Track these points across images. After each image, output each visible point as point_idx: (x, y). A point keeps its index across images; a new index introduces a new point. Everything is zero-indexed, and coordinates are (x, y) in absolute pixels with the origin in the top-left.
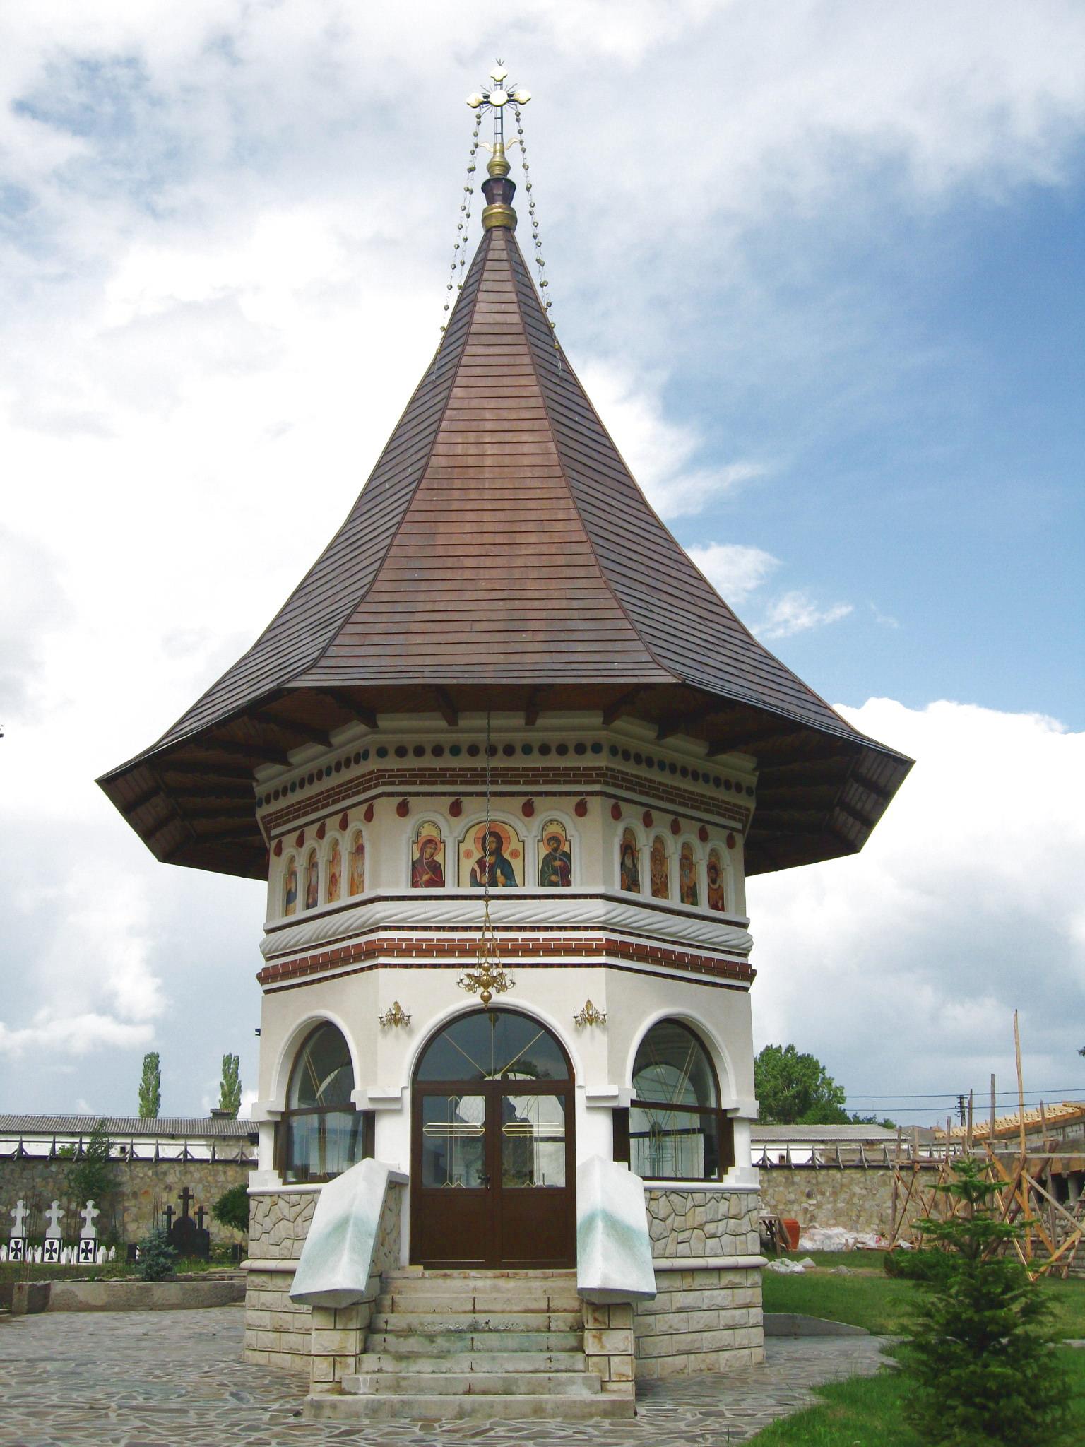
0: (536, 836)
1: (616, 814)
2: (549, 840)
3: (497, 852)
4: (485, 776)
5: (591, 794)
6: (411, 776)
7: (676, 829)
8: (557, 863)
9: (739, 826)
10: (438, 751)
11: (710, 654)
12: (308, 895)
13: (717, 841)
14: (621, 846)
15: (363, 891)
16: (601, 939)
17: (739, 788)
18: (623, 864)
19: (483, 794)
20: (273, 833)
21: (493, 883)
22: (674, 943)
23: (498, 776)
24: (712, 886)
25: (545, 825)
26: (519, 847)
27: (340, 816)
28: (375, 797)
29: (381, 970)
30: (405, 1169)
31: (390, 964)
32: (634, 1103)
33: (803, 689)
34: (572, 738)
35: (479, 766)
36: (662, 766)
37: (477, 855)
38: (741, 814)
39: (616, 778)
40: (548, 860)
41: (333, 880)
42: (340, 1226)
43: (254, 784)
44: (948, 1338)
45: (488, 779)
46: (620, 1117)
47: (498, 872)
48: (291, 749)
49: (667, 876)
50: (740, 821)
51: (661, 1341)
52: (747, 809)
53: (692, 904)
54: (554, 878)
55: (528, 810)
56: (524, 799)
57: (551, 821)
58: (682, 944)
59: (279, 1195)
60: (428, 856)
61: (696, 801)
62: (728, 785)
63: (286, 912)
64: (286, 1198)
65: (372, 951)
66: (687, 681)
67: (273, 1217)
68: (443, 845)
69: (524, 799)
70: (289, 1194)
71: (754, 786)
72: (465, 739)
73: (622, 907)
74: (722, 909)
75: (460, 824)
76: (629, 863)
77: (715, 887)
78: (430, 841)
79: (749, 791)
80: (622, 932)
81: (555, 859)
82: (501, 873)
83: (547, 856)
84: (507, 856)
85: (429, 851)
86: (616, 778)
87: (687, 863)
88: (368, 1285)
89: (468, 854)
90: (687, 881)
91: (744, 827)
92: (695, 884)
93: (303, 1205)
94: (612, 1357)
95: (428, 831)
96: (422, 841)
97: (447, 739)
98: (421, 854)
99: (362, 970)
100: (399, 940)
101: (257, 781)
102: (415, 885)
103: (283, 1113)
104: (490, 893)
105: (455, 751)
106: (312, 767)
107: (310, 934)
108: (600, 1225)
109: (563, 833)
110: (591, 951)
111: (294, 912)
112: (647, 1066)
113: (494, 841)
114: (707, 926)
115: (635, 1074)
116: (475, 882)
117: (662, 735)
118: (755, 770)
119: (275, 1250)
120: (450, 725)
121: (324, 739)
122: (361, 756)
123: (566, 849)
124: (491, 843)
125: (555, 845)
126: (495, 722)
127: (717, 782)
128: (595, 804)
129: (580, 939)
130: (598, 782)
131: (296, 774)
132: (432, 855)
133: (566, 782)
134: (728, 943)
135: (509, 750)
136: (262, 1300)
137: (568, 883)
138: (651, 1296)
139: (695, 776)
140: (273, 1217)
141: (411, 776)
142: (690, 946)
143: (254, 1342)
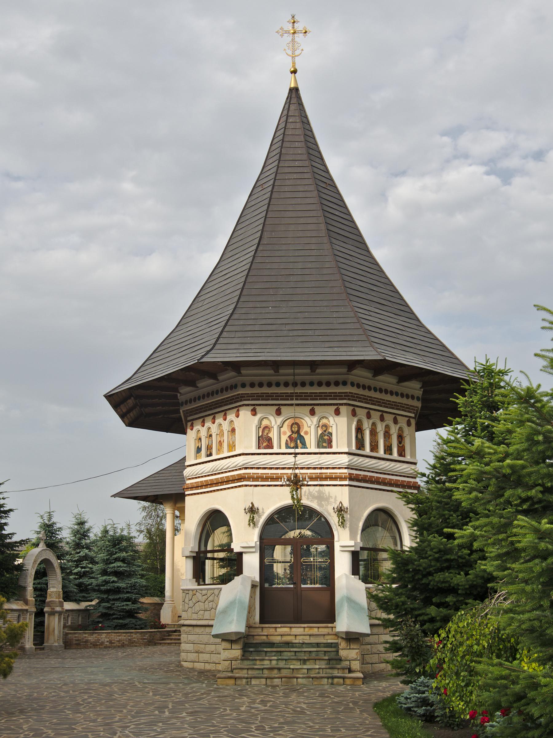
0: (316, 425)
1: (354, 414)
2: (323, 426)
3: (298, 432)
4: (293, 396)
5: (342, 404)
6: (257, 396)
7: (382, 419)
8: (326, 437)
9: (413, 415)
10: (270, 385)
11: (399, 336)
12: (207, 450)
14: (356, 428)
15: (235, 450)
16: (346, 473)
17: (413, 397)
18: (357, 437)
19: (292, 405)
20: (189, 418)
21: (297, 447)
22: (381, 473)
23: (299, 396)
24: (399, 445)
25: (320, 419)
26: (308, 430)
28: (240, 406)
30: (258, 579)
31: (248, 485)
32: (362, 548)
33: (445, 350)
34: (332, 378)
35: (289, 392)
36: (375, 390)
37: (289, 434)
38: (414, 410)
39: (354, 397)
40: (322, 435)
41: (220, 443)
42: (232, 604)
43: (179, 395)
45: (294, 395)
46: (355, 555)
47: (299, 441)
48: (198, 380)
49: (378, 442)
50: (413, 413)
51: (374, 657)
52: (417, 407)
53: (390, 454)
54: (324, 444)
56: (311, 407)
58: (385, 474)
59: (196, 590)
60: (266, 434)
61: (392, 405)
62: (407, 396)
63: (196, 458)
64: (200, 592)
66: (387, 358)
67: (194, 600)
68: (272, 429)
70: (201, 590)
71: (420, 396)
72: (282, 379)
73: (356, 458)
74: (404, 456)
75: (280, 420)
76: (359, 436)
77: (401, 445)
78: (266, 427)
79: (418, 399)
80: (356, 469)
81: (325, 435)
82: (300, 442)
83: (321, 434)
84: (302, 434)
85: (266, 431)
86: (354, 397)
87: (387, 435)
88: (246, 631)
89: (285, 433)
90: (387, 443)
91: (416, 415)
92: (391, 445)
93: (208, 595)
94: (351, 661)
95: (265, 423)
96: (262, 427)
97: (274, 379)
98: (263, 432)
99: (236, 487)
100: (253, 474)
101: (180, 393)
102: (259, 448)
103: (197, 552)
104: (296, 452)
105: (278, 385)
107: (209, 469)
108: (346, 605)
109: (329, 423)
110: (341, 479)
112: (368, 527)
115: (363, 530)
116: (287, 447)
117: (375, 375)
118: (421, 388)
119: (195, 616)
120: (275, 372)
122: (234, 387)
123: (330, 431)
124: (295, 429)
125: (325, 429)
126: (297, 371)
127: (402, 395)
128: (343, 409)
129: (337, 473)
130: (346, 399)
131: (201, 392)
132: (267, 434)
133: (330, 399)
135: (303, 384)
136: (189, 639)
137: (331, 447)
138: (368, 635)
139: (392, 393)
140: (194, 600)
141: (257, 396)
142: (389, 474)
143: (185, 658)
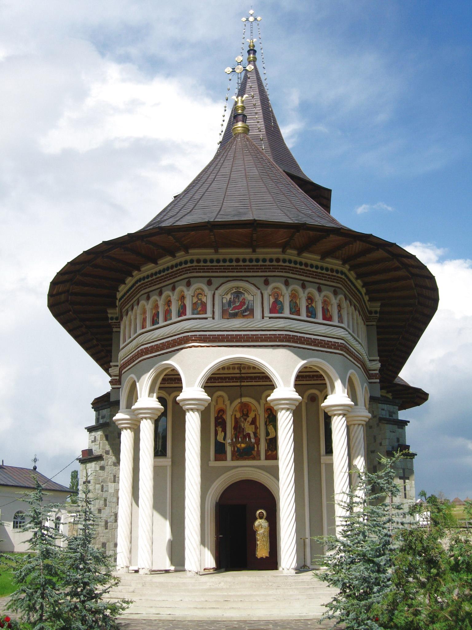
13: (327, 293)
27: (159, 290)
29: (193, 348)
34: (234, 257)
44: (240, 439)
55: (267, 283)
56: (264, 278)
57: (198, 289)
65: (187, 340)
69: (264, 278)
102: (193, 314)
106: (149, 273)
111: (146, 327)
113: (277, 296)
114: (335, 329)
121: (155, 262)
134: (214, 327)
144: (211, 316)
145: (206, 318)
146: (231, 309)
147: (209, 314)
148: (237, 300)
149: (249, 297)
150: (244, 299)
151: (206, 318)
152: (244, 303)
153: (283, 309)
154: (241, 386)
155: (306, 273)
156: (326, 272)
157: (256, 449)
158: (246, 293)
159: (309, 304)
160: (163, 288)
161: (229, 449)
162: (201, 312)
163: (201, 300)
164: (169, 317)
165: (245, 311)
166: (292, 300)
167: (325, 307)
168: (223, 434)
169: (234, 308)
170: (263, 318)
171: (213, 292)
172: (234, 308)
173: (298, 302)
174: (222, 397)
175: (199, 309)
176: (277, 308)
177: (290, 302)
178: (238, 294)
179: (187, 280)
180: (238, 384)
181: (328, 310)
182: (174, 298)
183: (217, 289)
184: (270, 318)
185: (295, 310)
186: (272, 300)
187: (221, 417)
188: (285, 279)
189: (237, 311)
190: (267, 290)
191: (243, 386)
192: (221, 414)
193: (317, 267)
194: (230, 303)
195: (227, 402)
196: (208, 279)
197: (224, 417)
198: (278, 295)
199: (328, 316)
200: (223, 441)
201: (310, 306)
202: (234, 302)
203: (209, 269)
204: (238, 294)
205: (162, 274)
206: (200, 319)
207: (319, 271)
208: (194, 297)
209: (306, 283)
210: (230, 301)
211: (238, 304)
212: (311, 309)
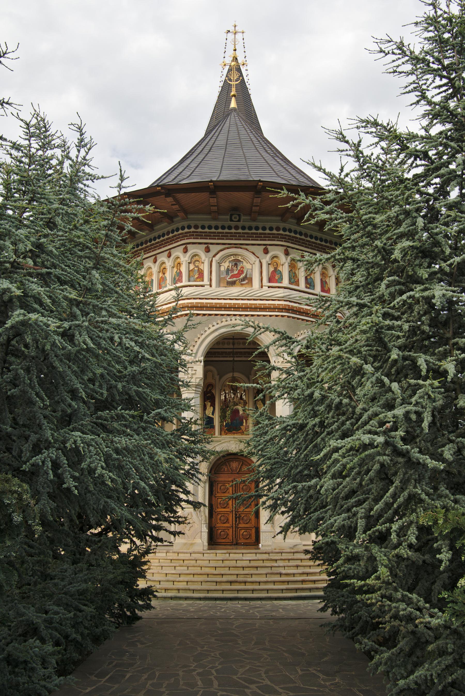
27: (154, 257)
102: (189, 281)
144: (209, 283)
145: (202, 286)
146: (229, 277)
147: (206, 281)
148: (235, 268)
149: (247, 266)
150: (243, 267)
151: (202, 286)
152: (243, 272)
153: (282, 279)
154: (234, 361)
155: (306, 244)
156: (320, 242)
157: (244, 424)
158: (245, 263)
159: (308, 275)
160: (172, 250)
161: (217, 423)
162: (198, 280)
163: (197, 267)
164: (163, 285)
165: (243, 279)
166: (291, 270)
167: (324, 280)
168: (212, 408)
169: (232, 276)
170: (262, 287)
171: (210, 259)
172: (232, 276)
173: (297, 272)
174: (211, 371)
175: (196, 276)
176: (277, 278)
177: (289, 272)
178: (236, 263)
179: (184, 246)
180: (231, 359)
181: (326, 282)
182: (169, 263)
183: (214, 256)
184: (269, 287)
185: (294, 279)
186: (272, 269)
187: (210, 392)
188: (285, 248)
189: (235, 279)
190: (265, 258)
191: (236, 361)
192: (210, 388)
193: (316, 238)
194: (228, 271)
195: (217, 377)
196: (206, 245)
197: (213, 392)
198: (277, 265)
199: (326, 289)
200: (211, 416)
201: (308, 277)
202: (232, 270)
203: (207, 236)
204: (236, 263)
205: (157, 240)
206: (196, 286)
207: (318, 242)
208: (191, 265)
209: (269, 247)
210: (228, 270)
211: (236, 272)
212: (309, 281)
